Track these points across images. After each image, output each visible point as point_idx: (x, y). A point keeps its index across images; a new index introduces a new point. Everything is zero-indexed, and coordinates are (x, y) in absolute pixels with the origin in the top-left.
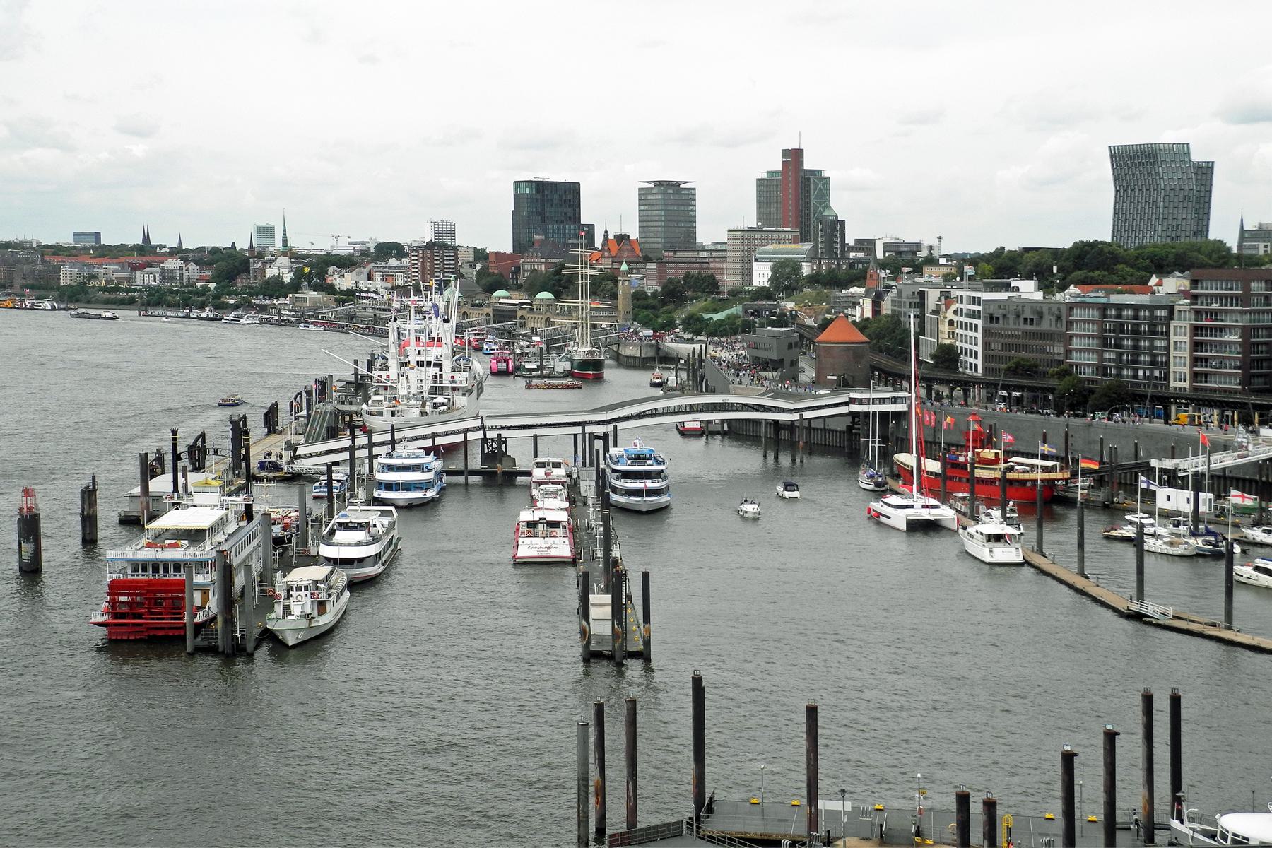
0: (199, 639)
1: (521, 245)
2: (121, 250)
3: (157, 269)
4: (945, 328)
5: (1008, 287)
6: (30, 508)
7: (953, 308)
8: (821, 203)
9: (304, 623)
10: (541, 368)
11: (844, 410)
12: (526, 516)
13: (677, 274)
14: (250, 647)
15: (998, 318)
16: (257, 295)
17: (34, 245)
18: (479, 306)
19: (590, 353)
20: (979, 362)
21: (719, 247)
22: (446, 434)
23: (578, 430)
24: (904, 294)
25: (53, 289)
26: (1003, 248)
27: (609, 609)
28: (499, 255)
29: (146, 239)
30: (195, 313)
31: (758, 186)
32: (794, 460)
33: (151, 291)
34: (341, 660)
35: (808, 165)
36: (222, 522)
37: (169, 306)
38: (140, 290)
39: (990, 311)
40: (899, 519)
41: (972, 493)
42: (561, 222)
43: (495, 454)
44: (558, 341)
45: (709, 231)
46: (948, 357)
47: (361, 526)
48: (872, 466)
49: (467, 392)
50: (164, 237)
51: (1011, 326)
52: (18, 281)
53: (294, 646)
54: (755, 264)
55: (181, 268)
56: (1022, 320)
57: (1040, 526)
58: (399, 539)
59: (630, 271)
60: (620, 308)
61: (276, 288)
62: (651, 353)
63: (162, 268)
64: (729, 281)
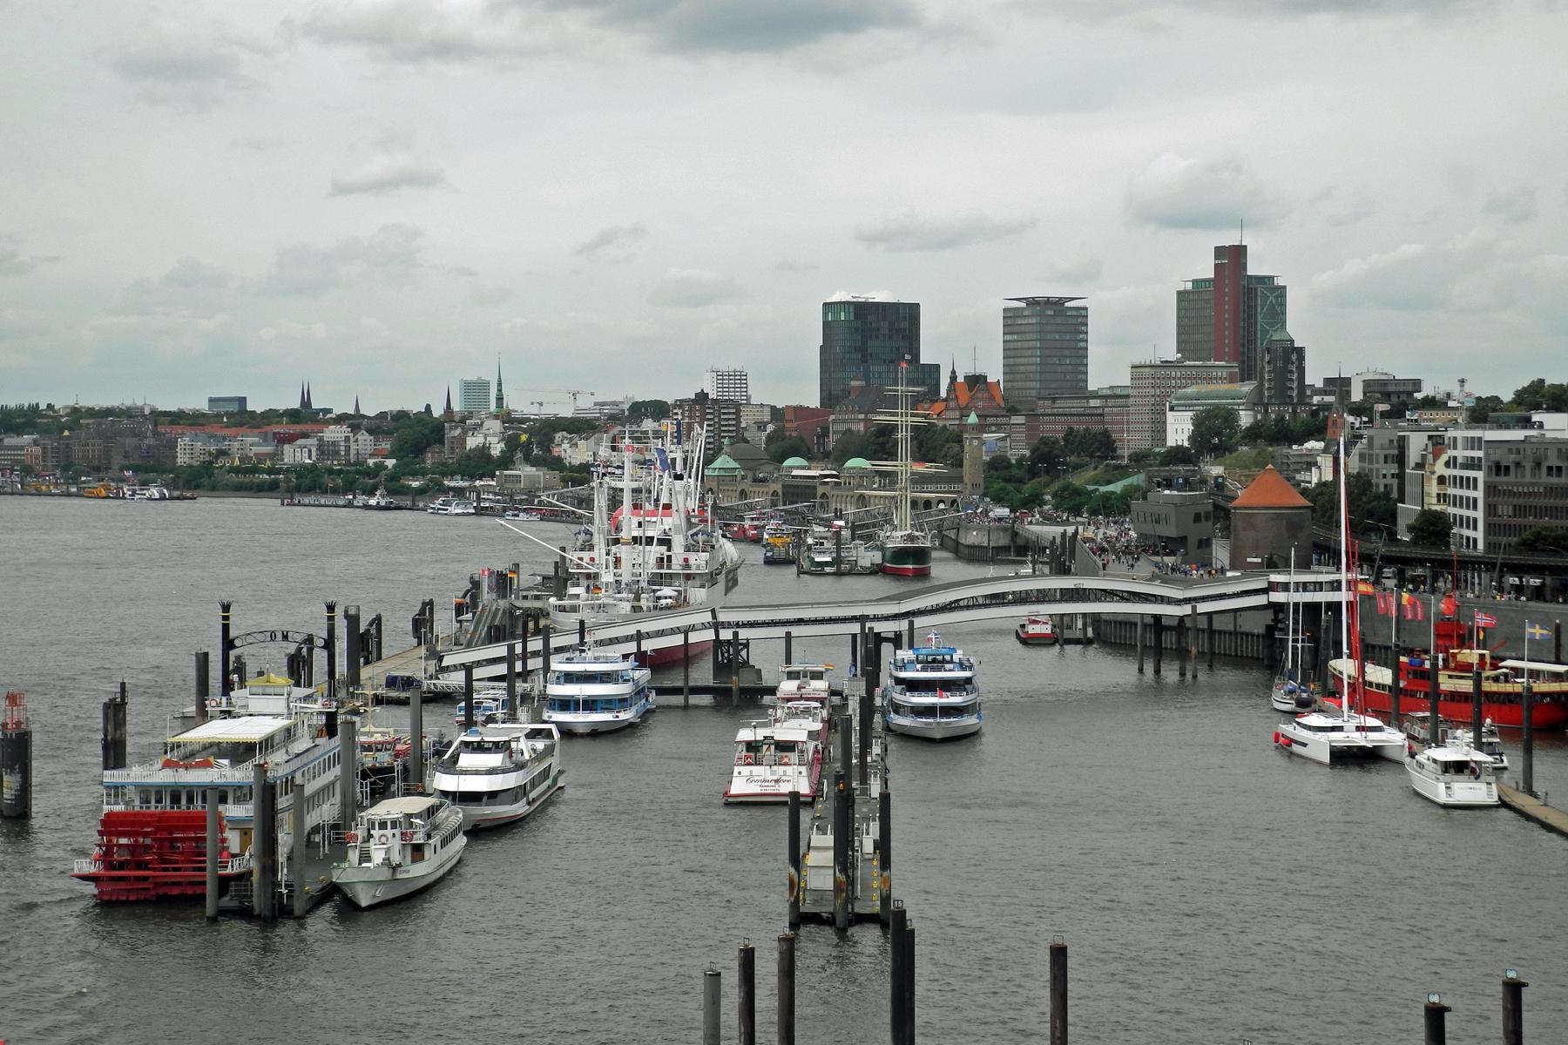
0: (226, 898)
1: (830, 398)
2: (271, 416)
3: (313, 441)
4: (1433, 488)
5: (1526, 423)
6: (18, 724)
7: (1444, 458)
8: (1272, 325)
9: (385, 874)
10: (837, 561)
11: (1261, 600)
12: (745, 735)
13: (1055, 430)
14: (299, 907)
15: (1507, 468)
16: (452, 474)
17: (147, 412)
18: (763, 480)
19: (911, 538)
20: (1479, 535)
21: (1119, 392)
22: (661, 633)
23: (855, 628)
24: (1376, 443)
25: (164, 471)
26: (1542, 381)
27: (831, 853)
28: (799, 410)
29: (306, 403)
30: (361, 499)
31: (1179, 301)
32: (1183, 674)
33: (300, 471)
34: (450, 937)
35: (1254, 268)
36: (289, 734)
37: (325, 491)
38: (288, 471)
39: (1497, 458)
40: (1319, 747)
41: (1435, 710)
42: (892, 362)
43: (729, 657)
44: (866, 526)
45: (1106, 369)
46: (1434, 528)
47: (497, 747)
48: (1292, 677)
49: (711, 579)
50: (332, 398)
51: (1528, 478)
52: (117, 460)
53: (371, 908)
54: (1169, 414)
55: (347, 439)
56: (1544, 470)
57: (1528, 752)
58: (560, 772)
59: (981, 428)
60: (966, 479)
61: (480, 464)
62: (1002, 540)
63: (321, 439)
64: (1131, 440)
